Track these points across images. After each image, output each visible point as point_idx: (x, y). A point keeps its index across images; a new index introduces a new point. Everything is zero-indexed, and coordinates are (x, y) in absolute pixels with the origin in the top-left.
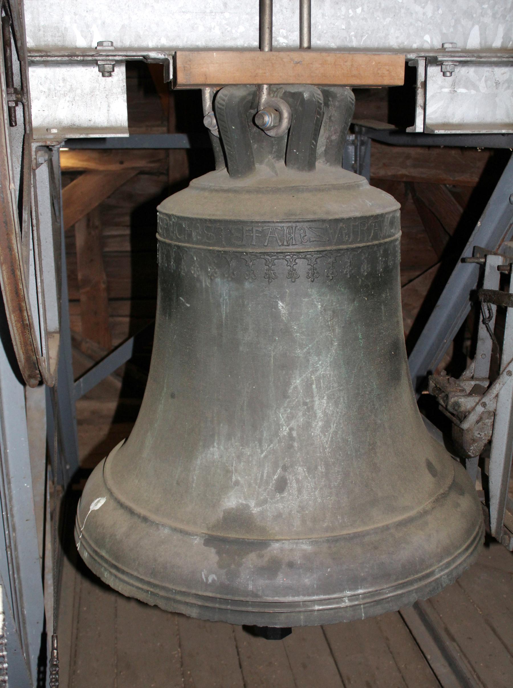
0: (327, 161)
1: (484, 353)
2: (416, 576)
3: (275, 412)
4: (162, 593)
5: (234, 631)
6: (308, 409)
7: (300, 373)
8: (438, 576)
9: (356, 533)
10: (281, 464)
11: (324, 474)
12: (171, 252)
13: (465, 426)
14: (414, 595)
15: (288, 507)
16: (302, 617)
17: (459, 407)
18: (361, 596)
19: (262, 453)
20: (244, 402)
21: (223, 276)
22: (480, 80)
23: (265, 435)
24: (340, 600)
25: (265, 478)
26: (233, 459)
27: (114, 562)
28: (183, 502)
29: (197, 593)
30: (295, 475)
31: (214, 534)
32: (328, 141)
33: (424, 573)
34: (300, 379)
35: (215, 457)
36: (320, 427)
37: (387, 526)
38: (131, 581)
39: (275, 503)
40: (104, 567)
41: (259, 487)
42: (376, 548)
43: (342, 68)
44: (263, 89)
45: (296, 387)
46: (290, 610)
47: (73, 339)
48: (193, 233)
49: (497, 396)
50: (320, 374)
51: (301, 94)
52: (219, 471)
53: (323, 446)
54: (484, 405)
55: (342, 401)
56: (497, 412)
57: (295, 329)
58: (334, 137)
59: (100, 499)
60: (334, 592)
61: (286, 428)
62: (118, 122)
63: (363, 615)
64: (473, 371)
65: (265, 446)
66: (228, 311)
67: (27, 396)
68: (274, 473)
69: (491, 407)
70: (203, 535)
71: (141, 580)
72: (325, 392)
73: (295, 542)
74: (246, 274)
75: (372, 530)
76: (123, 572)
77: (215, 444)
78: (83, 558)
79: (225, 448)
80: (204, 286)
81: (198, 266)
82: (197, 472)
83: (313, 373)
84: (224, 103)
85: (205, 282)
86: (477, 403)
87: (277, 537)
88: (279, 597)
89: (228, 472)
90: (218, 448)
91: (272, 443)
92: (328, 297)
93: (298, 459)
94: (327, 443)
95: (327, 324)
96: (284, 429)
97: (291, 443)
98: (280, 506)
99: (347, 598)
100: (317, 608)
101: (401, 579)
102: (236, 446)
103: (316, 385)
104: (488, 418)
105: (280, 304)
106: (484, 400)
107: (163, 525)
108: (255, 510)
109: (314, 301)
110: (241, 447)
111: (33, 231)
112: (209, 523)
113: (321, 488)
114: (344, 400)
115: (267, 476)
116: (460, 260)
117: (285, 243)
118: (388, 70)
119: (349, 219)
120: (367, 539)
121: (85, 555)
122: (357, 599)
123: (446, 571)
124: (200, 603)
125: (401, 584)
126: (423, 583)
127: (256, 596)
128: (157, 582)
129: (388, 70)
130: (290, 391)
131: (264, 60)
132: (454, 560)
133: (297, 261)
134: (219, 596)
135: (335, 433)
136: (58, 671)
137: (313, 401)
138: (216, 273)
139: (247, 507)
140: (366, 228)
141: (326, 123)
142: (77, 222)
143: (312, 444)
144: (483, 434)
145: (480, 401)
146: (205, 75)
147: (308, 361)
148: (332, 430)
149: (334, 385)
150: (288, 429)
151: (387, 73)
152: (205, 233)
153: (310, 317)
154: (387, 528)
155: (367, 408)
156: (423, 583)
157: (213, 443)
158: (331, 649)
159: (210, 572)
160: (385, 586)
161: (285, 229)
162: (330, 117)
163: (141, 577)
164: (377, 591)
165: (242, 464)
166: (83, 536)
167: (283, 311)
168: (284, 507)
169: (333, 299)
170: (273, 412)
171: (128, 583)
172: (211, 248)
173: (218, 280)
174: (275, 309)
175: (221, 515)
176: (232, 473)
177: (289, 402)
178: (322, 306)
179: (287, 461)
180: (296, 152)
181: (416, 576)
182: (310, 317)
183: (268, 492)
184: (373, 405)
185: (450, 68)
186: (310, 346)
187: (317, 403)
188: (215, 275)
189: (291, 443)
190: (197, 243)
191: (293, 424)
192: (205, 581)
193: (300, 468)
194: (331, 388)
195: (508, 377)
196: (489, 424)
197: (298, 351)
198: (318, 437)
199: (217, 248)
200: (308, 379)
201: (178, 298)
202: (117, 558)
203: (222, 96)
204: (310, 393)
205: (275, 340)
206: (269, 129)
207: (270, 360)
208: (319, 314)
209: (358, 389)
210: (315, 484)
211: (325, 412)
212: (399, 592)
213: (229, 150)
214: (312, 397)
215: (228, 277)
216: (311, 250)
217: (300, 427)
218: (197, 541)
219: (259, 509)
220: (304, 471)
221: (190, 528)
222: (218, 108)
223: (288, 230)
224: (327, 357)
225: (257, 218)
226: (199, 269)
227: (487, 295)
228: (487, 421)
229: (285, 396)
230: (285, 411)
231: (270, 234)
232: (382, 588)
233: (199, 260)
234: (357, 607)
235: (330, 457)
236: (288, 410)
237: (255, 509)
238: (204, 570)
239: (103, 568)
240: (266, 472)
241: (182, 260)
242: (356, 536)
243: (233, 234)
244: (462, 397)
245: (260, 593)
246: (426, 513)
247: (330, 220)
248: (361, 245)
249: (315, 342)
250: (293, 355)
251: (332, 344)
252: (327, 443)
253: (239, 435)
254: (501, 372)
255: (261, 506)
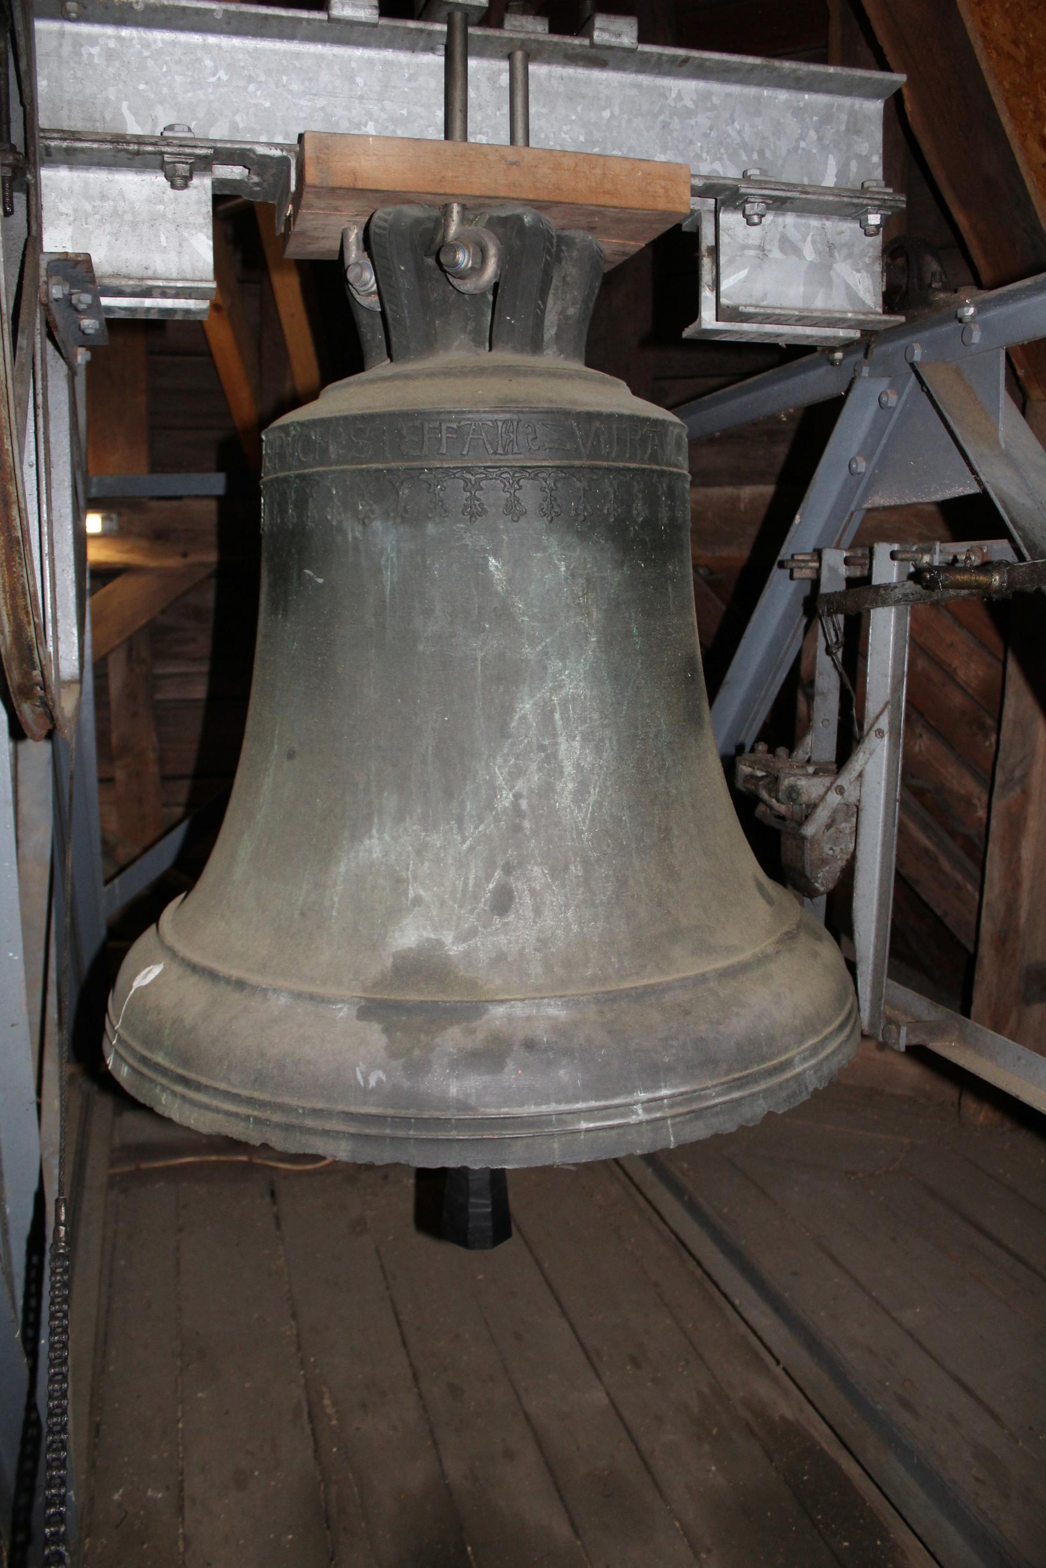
0: (561, 351)
1: (827, 717)
2: (763, 1066)
3: (487, 765)
4: (277, 1118)
5: (388, 1288)
6: (548, 759)
7: (531, 691)
8: (799, 1069)
9: (649, 985)
10: (500, 861)
11: (582, 879)
12: (288, 492)
13: (810, 830)
14: (761, 1101)
15: (517, 941)
16: (556, 1146)
17: (798, 794)
18: (665, 1101)
19: (464, 842)
20: (427, 748)
21: (386, 517)
22: (804, 240)
23: (468, 808)
24: (627, 1109)
25: (470, 889)
26: (409, 856)
27: (180, 1071)
28: (313, 946)
29: (346, 1109)
30: (528, 881)
31: (378, 996)
32: (561, 317)
33: (775, 1062)
34: (531, 702)
35: (375, 856)
36: (570, 793)
37: (703, 975)
38: (215, 1103)
39: (491, 934)
40: (161, 1084)
41: (461, 907)
42: (687, 1013)
43: (587, 178)
44: (452, 212)
45: (524, 717)
46: (531, 1132)
47: (105, 842)
48: (331, 447)
49: (860, 775)
50: (567, 694)
51: (519, 218)
52: (381, 881)
53: (577, 827)
54: (841, 790)
55: (608, 745)
56: (861, 806)
57: (519, 609)
58: (571, 311)
59: (151, 967)
60: (616, 1095)
61: (508, 794)
62: (197, 272)
63: (672, 1139)
64: (809, 750)
65: (470, 828)
66: (395, 579)
67: (20, 838)
68: (488, 878)
69: (852, 795)
70: (356, 1000)
71: (235, 1098)
72: (577, 727)
73: (534, 1003)
74: (430, 508)
75: (678, 981)
76: (198, 1087)
77: (374, 832)
78: (120, 1080)
79: (392, 838)
80: (350, 539)
81: (339, 504)
82: (339, 888)
83: (555, 691)
84: (386, 225)
85: (353, 531)
86: (829, 789)
87: (500, 997)
88: (509, 1106)
89: (398, 882)
90: (380, 839)
91: (482, 822)
92: (578, 552)
93: (532, 851)
94: (584, 822)
95: (577, 601)
96: (504, 796)
97: (517, 821)
98: (502, 939)
99: (640, 1105)
100: (584, 1125)
101: (737, 1071)
102: (414, 831)
103: (561, 714)
104: (845, 821)
105: (492, 561)
106: (839, 782)
107: (275, 990)
108: (455, 950)
109: (552, 558)
110: (424, 834)
111: (36, 416)
112: (366, 979)
113: (577, 906)
114: (611, 743)
115: (476, 885)
116: (775, 567)
117: (500, 451)
118: (663, 187)
119: (610, 416)
120: (668, 998)
121: (123, 1074)
122: (660, 1108)
123: (813, 1062)
124: (352, 1130)
125: (738, 1079)
126: (775, 1080)
127: (465, 1107)
128: (265, 1097)
129: (663, 187)
130: (513, 724)
131: (455, 156)
132: (823, 1043)
133: (522, 482)
134: (390, 1112)
135: (599, 804)
136: (65, 1459)
137: (556, 744)
138: (373, 512)
139: (440, 943)
140: (639, 437)
141: (556, 289)
142: (111, 651)
143: (557, 824)
144: (837, 849)
145: (832, 784)
146: (354, 174)
147: (545, 668)
148: (592, 799)
149: (593, 715)
150: (511, 795)
151: (661, 191)
152: (353, 441)
153: (547, 587)
154: (702, 979)
155: (652, 763)
156: (775, 1080)
157: (370, 830)
158: (561, 1306)
159: (372, 1066)
160: (709, 1083)
161: (500, 424)
162: (564, 278)
163: (235, 1091)
164: (695, 1091)
165: (427, 864)
166: (120, 1040)
167: (498, 575)
168: (510, 942)
169: (586, 556)
170: (483, 764)
171: (207, 1107)
172: (364, 466)
173: (377, 525)
174: (483, 572)
175: (389, 962)
176: (408, 883)
177: (513, 744)
178: (567, 568)
179: (511, 856)
180: (510, 321)
181: (763, 1066)
182: (547, 587)
183: (478, 914)
184: (663, 760)
185: (759, 209)
186: (548, 640)
187: (563, 747)
188: (372, 516)
189: (517, 821)
190: (338, 462)
191: (520, 785)
192: (362, 1084)
193: (536, 869)
194: (588, 721)
195: (879, 741)
196: (847, 831)
197: (527, 650)
198: (568, 810)
199: (375, 466)
200: (545, 703)
201: (300, 574)
202: (186, 1061)
203: (382, 215)
204: (550, 728)
205: (484, 628)
206: (462, 276)
207: (476, 666)
208: (563, 582)
209: (636, 728)
210: (566, 898)
211: (579, 764)
212: (736, 1095)
213: (394, 312)
214: (555, 736)
215: (394, 518)
216: (547, 464)
217: (533, 792)
218: (344, 1012)
219: (462, 947)
220: (545, 875)
221: (330, 991)
222: (375, 233)
223: (504, 426)
224: (578, 662)
225: (449, 407)
226: (341, 509)
227: (832, 603)
228: (843, 825)
229: (504, 732)
230: (506, 761)
231: (473, 434)
232: (705, 1085)
233: (341, 493)
234: (661, 1123)
235: (590, 849)
236: (510, 760)
237: (455, 948)
238: (361, 1063)
239: (159, 1087)
240: (472, 877)
241: (310, 500)
242: (648, 991)
243: (405, 437)
244: (803, 778)
245: (472, 1101)
246: (763, 959)
247: (579, 414)
248: (633, 465)
249: (557, 633)
250: (518, 656)
251: (587, 639)
252: (584, 822)
253: (419, 811)
254: (865, 732)
255: (464, 941)
